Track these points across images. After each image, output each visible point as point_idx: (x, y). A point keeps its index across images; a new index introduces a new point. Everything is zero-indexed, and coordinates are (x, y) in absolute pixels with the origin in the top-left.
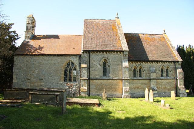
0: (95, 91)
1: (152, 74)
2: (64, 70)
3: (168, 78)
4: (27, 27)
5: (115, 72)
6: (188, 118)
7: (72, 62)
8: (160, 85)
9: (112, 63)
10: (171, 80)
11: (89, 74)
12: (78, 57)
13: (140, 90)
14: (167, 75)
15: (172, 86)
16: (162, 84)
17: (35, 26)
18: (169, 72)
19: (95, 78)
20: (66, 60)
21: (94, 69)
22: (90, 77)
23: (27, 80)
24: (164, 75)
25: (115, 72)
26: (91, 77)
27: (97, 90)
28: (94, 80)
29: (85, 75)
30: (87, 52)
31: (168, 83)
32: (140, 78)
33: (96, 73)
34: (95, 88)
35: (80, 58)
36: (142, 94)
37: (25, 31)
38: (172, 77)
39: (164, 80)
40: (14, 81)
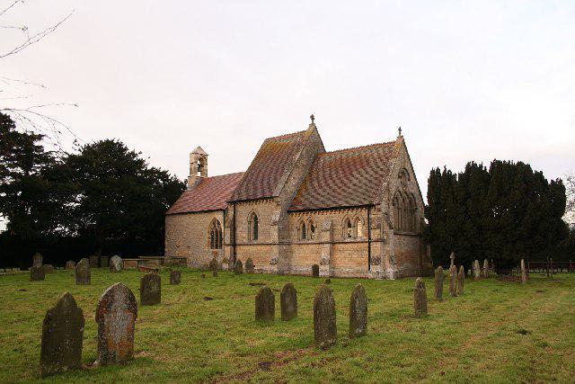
20: (208, 218)
26: (238, 242)
29: (227, 239)
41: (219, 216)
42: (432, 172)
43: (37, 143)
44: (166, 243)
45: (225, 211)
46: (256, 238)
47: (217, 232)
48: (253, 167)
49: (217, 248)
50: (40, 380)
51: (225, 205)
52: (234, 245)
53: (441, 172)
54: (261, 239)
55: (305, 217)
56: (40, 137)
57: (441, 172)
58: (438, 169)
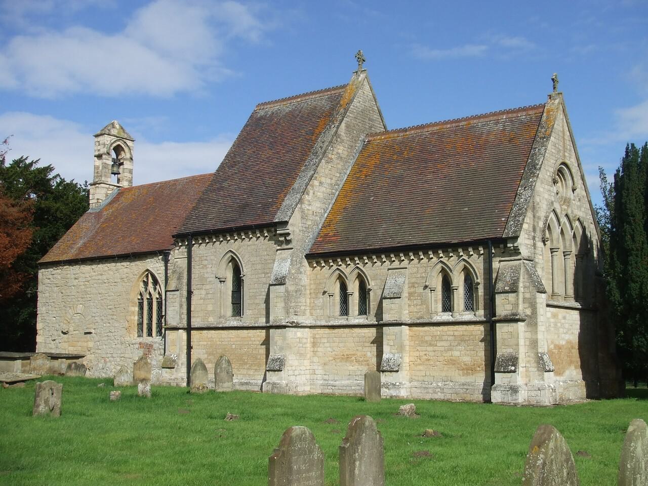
26: (195, 323)
40: (39, 339)
41: (155, 265)
44: (39, 326)
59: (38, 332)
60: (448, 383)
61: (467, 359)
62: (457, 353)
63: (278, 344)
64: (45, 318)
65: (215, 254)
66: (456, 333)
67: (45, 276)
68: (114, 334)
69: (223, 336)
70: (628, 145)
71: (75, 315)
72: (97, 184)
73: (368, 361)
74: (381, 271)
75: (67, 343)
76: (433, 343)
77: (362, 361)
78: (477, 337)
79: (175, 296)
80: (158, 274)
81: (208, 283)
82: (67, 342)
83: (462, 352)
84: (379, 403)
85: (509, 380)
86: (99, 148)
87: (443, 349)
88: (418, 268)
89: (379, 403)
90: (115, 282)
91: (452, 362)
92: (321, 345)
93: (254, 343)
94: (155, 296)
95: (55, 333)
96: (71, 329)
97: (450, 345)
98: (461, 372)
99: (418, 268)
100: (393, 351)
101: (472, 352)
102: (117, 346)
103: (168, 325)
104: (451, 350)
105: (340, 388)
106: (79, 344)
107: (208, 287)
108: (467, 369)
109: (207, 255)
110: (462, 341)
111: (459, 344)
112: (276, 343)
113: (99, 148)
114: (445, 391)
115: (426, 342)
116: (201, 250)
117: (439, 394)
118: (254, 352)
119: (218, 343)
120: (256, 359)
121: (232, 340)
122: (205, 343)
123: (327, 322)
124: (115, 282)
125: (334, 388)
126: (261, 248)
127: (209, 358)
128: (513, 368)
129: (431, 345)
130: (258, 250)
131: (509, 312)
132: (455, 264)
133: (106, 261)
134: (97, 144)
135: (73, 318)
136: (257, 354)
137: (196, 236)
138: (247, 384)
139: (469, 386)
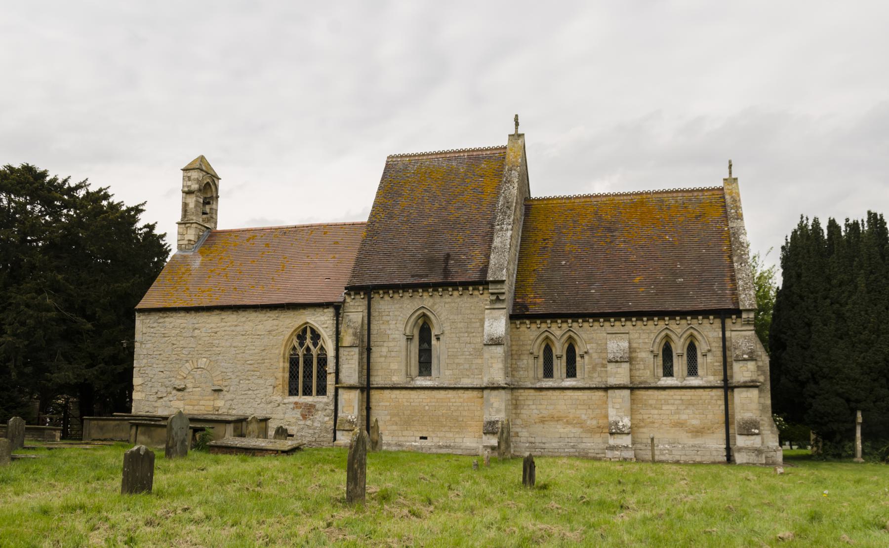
0: (389, 428)
1: (611, 367)
2: (287, 355)
3: (693, 381)
4: (185, 205)
5: (457, 361)
6: (487, 470)
7: (313, 331)
8: (656, 412)
9: (447, 327)
10: (707, 392)
11: (367, 368)
12: (330, 312)
13: (569, 429)
14: (693, 371)
15: (710, 416)
16: (664, 407)
17: (217, 197)
18: (700, 359)
19: (388, 383)
20: (291, 322)
21: (385, 350)
22: (372, 379)
23: (174, 392)
24: (676, 368)
25: (457, 361)
26: (378, 380)
27: (394, 427)
28: (387, 392)
29: (350, 372)
30: (362, 293)
31: (690, 404)
32: (569, 382)
33: (394, 366)
34: (388, 418)
35: (337, 315)
36: (573, 447)
37: (179, 220)
38: (711, 378)
39: (672, 392)
40: (136, 396)
41: (322, 321)
42: (802, 227)
43: (66, 186)
44: (137, 381)
45: (338, 308)
46: (425, 365)
47: (308, 362)
48: (373, 215)
49: (307, 392)
50: (194, 547)
51: (338, 296)
52: (366, 389)
53: (48, 179)
54: (442, 374)
55: (558, 331)
56: (830, 218)
57: (48, 179)
58: (816, 223)
59: (134, 387)
60: (675, 445)
61: (695, 422)
62: (684, 417)
63: (494, 406)
64: (147, 372)
65: (401, 310)
66: (683, 397)
67: (141, 324)
68: (255, 392)
69: (412, 396)
70: (802, 218)
71: (195, 370)
72: (189, 223)
73: (582, 423)
74: (598, 335)
75: (182, 402)
76: (658, 406)
77: (576, 423)
78: (706, 401)
79: (353, 353)
80: (323, 328)
81: (390, 340)
82: (182, 400)
83: (690, 416)
84: (44, 530)
85: (752, 442)
86: (189, 183)
87: (668, 412)
88: (640, 333)
89: (44, 530)
90: (258, 335)
91: (680, 425)
92: (525, 407)
93: (454, 404)
94: (315, 351)
95: (163, 389)
96: (189, 385)
97: (677, 409)
98: (690, 435)
99: (640, 333)
100: (619, 414)
101: (702, 416)
102: (261, 405)
103: (341, 383)
104: (679, 413)
105: (550, 450)
106: (202, 403)
107: (391, 344)
108: (697, 432)
109: (389, 310)
110: (690, 405)
111: (687, 408)
112: (492, 404)
113: (189, 183)
114: (673, 453)
115: (651, 405)
116: (385, 305)
117: (667, 455)
118: (454, 414)
119: (406, 404)
120: (458, 421)
121: (424, 401)
122: (388, 404)
123: (532, 383)
124: (258, 335)
125: (543, 450)
126: (463, 305)
127: (393, 419)
128: (757, 431)
129: (655, 408)
130: (459, 308)
131: (748, 379)
132: (679, 330)
133: (243, 311)
134: (187, 179)
135: (192, 373)
136: (458, 416)
137: (375, 289)
138: (447, 447)
139: (700, 447)
